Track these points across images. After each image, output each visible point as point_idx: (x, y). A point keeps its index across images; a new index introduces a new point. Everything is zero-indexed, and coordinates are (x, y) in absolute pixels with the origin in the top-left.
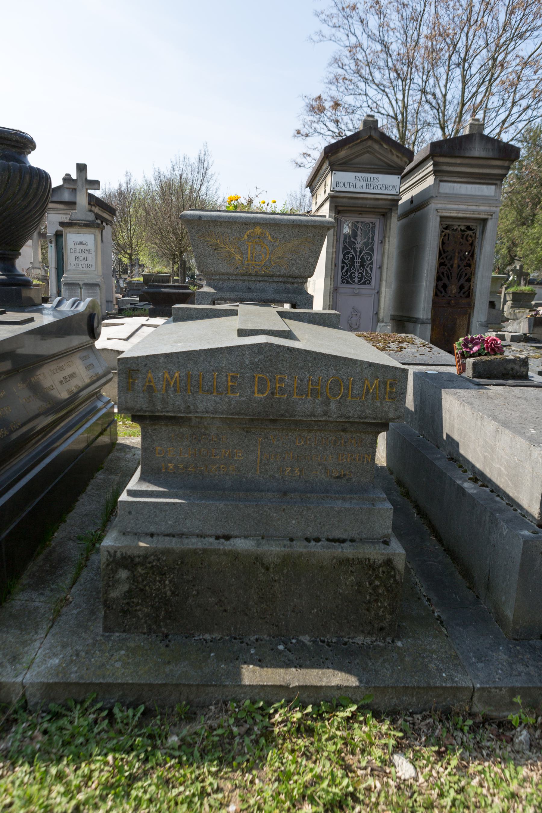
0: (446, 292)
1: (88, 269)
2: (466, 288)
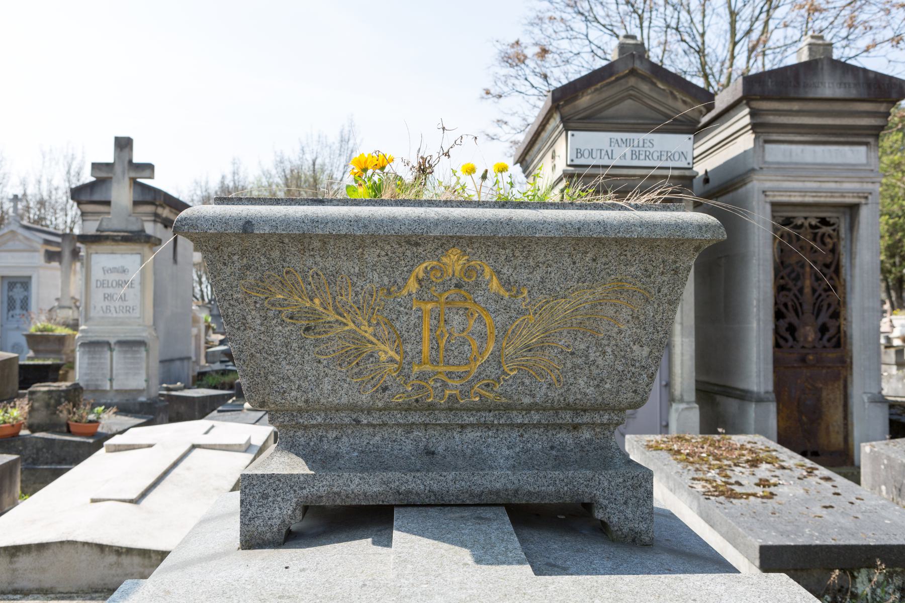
0: (794, 339)
1: (128, 315)
2: (832, 331)
